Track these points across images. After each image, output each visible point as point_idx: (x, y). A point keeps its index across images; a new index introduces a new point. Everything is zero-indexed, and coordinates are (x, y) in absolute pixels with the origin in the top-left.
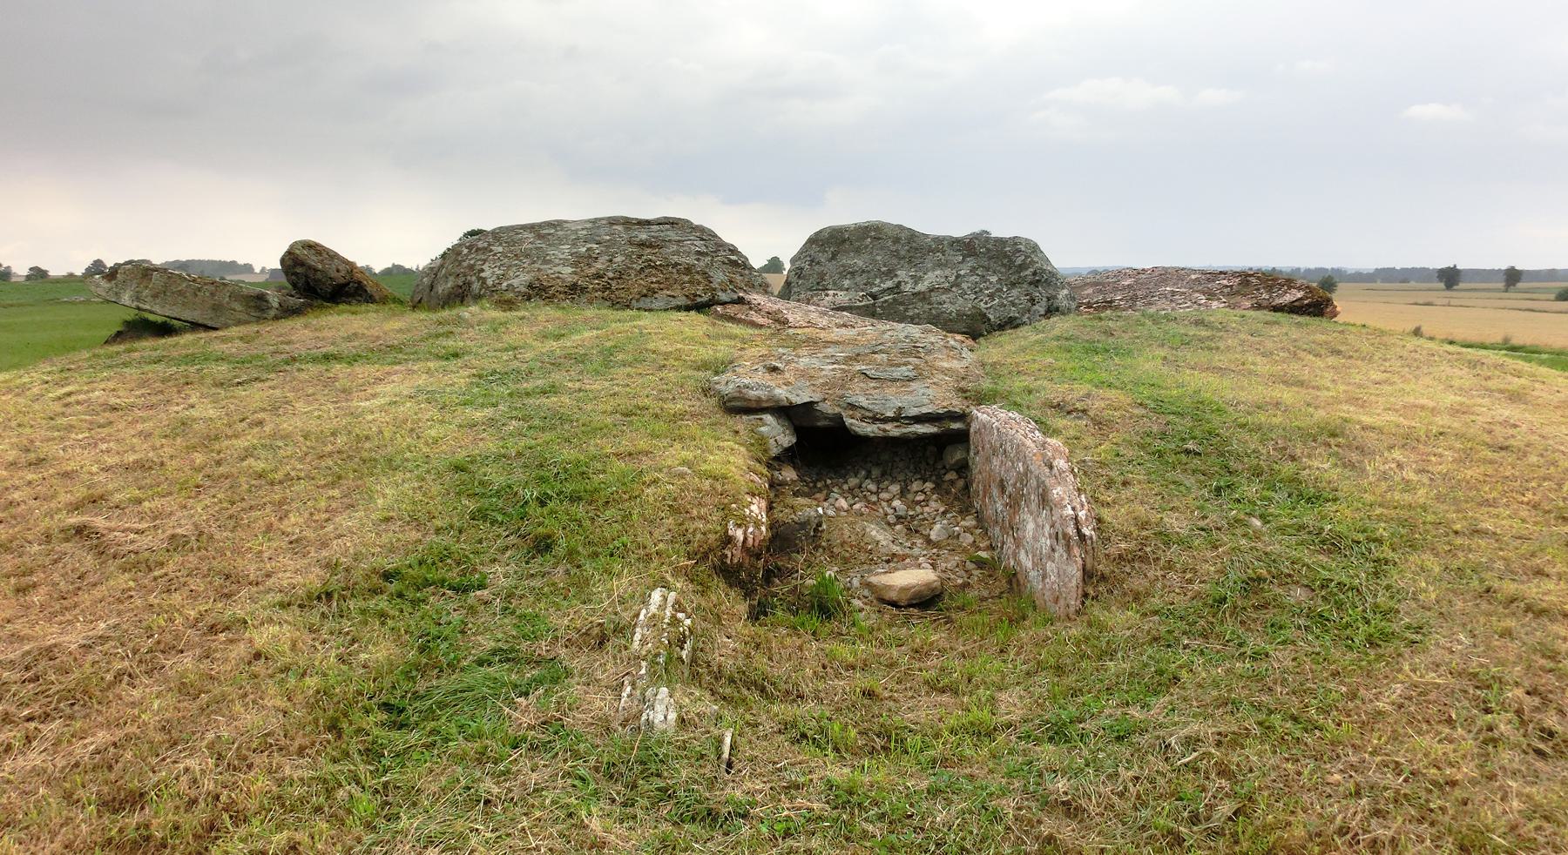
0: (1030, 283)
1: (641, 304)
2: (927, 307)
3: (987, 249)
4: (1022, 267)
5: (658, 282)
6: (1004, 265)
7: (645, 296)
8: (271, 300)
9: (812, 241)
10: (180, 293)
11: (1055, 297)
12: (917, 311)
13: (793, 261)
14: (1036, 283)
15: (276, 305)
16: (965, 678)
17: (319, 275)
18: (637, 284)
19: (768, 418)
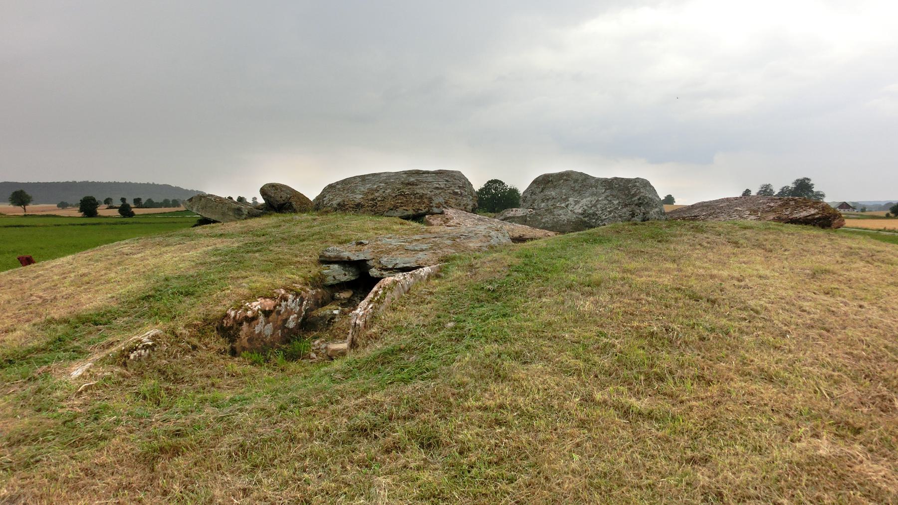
0: (636, 205)
1: (388, 214)
2: (552, 217)
3: (620, 186)
4: (634, 195)
5: (402, 203)
6: (625, 194)
7: (392, 209)
8: (243, 211)
9: (535, 182)
10: (211, 207)
11: (648, 213)
12: (547, 219)
13: (524, 193)
14: (639, 205)
15: (246, 213)
16: (852, 464)
17: (272, 200)
18: (389, 203)
19: (336, 266)
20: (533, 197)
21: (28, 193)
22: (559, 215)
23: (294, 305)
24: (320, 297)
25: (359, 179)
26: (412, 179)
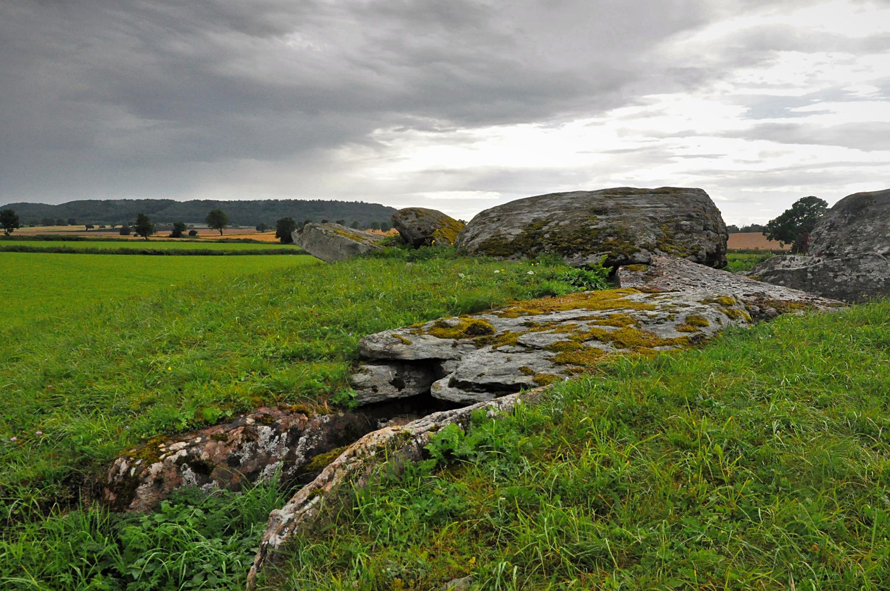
12: (845, 278)
20: (833, 234)
21: (227, 213)
22: (869, 271)
23: (273, 445)
24: (341, 426)
25: (99, 204)
26: (610, 203)
